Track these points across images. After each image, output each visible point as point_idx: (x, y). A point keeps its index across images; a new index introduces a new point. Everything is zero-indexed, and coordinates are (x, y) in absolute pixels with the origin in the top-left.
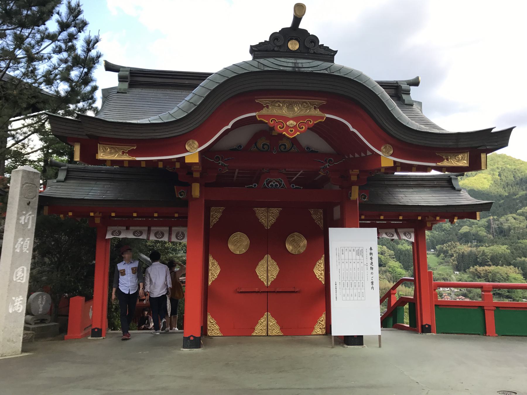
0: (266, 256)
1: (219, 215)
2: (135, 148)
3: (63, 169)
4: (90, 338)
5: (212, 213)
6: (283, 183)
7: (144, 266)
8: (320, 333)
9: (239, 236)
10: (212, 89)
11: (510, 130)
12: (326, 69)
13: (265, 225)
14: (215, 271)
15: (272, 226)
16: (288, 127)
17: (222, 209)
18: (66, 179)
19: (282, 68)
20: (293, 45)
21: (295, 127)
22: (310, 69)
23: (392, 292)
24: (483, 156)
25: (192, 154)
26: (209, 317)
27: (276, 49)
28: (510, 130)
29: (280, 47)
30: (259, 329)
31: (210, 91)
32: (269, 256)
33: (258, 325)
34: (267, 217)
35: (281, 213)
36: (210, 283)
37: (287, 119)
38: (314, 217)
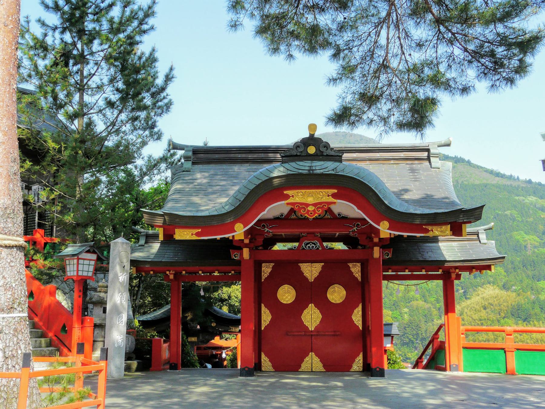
0: (310, 305)
1: (269, 270)
2: (200, 230)
3: (142, 235)
4: (168, 371)
5: (263, 269)
6: (318, 244)
7: (97, 226)
8: (357, 370)
9: (286, 288)
10: (251, 189)
11: (482, 207)
12: (333, 170)
13: (309, 278)
14: (266, 317)
15: (315, 279)
16: (308, 211)
17: (272, 264)
18: (146, 242)
19: (300, 171)
20: (312, 150)
21: (314, 211)
22: (322, 171)
23: (436, 337)
24: (463, 225)
25: (239, 232)
26: (263, 356)
27: (298, 154)
28: (482, 207)
29: (301, 152)
30: (305, 365)
31: (249, 191)
32: (313, 305)
33: (304, 363)
34: (311, 271)
35: (323, 267)
36: (263, 329)
37: (308, 205)
38: (353, 270)
